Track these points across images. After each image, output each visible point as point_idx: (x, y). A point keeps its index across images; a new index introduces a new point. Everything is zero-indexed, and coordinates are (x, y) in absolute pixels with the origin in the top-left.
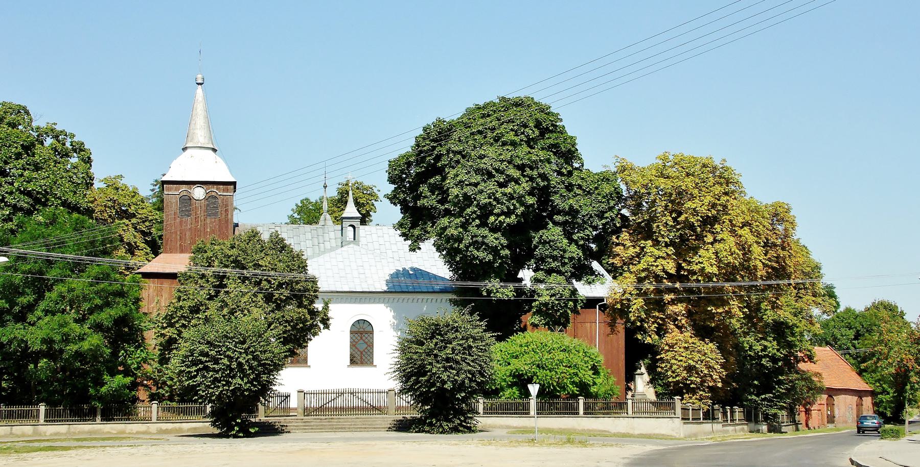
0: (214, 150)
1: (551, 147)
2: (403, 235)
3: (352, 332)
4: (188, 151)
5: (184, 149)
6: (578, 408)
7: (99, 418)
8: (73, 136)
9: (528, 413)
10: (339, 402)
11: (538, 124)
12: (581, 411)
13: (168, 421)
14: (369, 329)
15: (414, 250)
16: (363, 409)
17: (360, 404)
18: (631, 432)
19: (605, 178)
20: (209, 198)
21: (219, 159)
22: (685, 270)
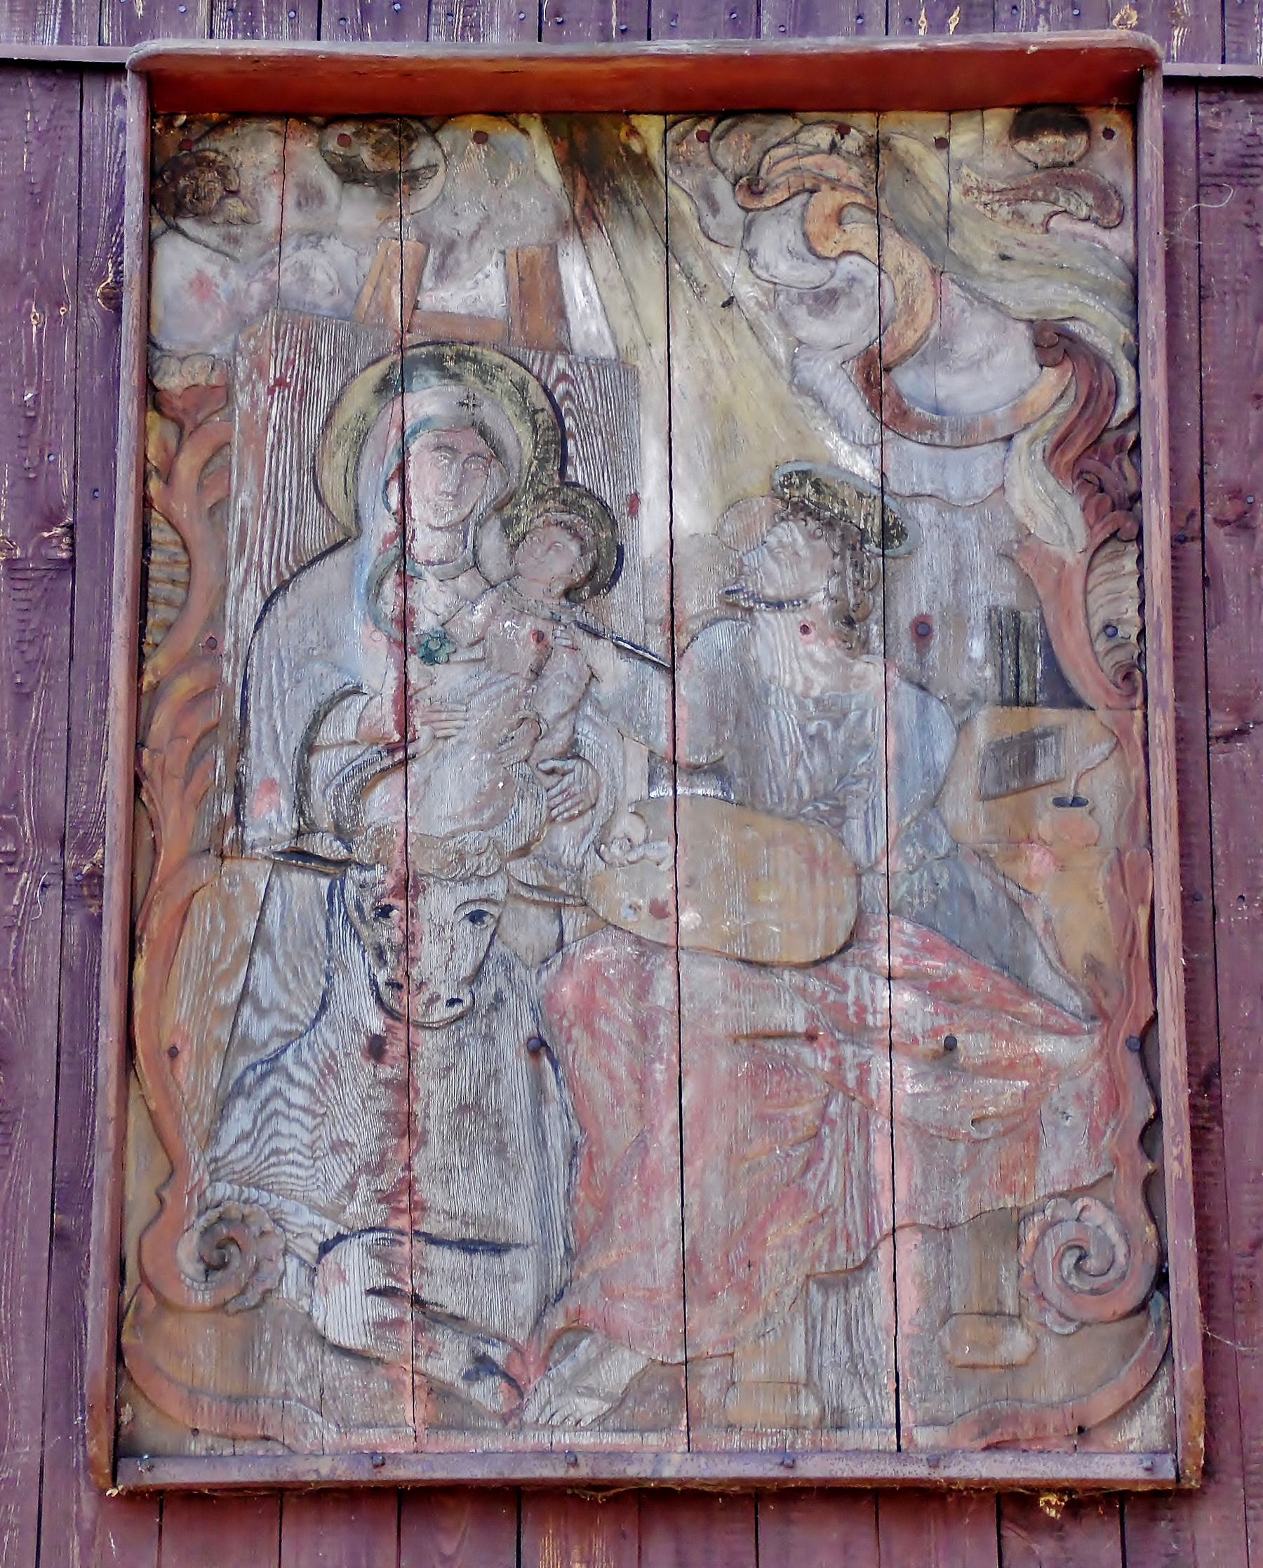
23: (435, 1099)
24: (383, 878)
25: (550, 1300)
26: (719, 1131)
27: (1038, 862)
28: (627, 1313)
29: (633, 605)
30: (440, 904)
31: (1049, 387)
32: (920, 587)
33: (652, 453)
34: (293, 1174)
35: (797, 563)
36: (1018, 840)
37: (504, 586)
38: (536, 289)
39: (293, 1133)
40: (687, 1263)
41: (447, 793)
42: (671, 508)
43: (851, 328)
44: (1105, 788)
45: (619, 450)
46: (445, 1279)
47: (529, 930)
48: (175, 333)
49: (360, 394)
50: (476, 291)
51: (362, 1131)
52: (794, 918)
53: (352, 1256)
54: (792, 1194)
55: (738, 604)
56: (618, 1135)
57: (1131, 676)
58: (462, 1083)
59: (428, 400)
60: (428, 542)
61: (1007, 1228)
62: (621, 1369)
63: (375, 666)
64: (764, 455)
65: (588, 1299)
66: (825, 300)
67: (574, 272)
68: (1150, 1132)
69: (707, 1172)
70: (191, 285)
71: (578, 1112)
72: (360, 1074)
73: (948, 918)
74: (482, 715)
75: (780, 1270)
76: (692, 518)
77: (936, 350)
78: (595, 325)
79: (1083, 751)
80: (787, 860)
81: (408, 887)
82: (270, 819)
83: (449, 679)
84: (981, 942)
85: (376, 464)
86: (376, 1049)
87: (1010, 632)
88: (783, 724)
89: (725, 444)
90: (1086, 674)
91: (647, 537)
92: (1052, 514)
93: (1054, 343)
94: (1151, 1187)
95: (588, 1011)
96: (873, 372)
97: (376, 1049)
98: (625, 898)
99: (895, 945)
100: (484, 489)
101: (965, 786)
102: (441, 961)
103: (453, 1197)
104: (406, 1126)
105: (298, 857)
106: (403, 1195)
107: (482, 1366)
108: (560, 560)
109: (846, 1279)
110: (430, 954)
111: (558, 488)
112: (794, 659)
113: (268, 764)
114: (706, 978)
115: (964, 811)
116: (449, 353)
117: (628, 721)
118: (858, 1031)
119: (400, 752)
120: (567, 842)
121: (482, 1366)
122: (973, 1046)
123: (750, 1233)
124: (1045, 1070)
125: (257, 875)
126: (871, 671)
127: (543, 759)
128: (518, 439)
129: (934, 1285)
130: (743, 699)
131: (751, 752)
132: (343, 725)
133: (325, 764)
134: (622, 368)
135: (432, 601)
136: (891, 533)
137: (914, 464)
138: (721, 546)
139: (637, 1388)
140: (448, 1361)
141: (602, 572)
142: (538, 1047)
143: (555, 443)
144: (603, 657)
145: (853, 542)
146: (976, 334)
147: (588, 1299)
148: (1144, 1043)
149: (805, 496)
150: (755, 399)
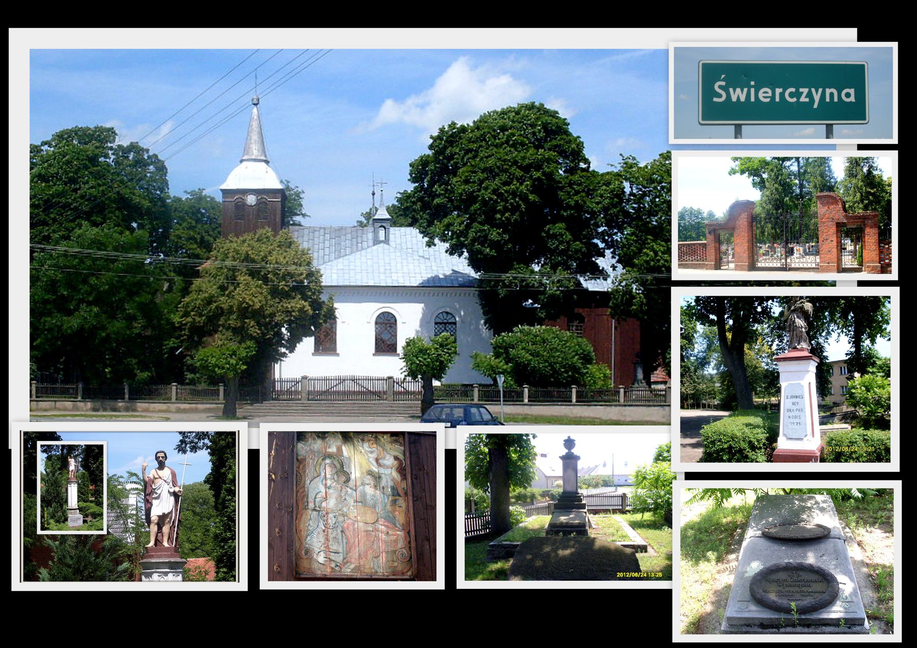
0: (267, 162)
1: (554, 148)
2: (421, 232)
3: (376, 323)
4: (244, 163)
5: (242, 161)
6: (571, 397)
7: (823, 414)
8: (147, 151)
9: (571, 401)
10: (341, 388)
11: (545, 126)
12: (574, 400)
13: (185, 401)
14: (393, 321)
15: (430, 246)
16: (359, 393)
17: (357, 389)
18: (622, 419)
19: (608, 179)
20: (259, 203)
21: (269, 169)
22: (569, 207)
23: (331, 536)
24: (324, 513)
25: (344, 559)
26: (363, 541)
27: (397, 513)
28: (353, 560)
29: (351, 484)
30: (331, 515)
31: (396, 462)
32: (383, 483)
33: (208, 406)
34: (315, 544)
35: (369, 480)
36: (394, 511)
37: (337, 481)
38: (339, 449)
39: (315, 540)
40: (360, 555)
41: (331, 503)
42: (356, 473)
43: (374, 455)
44: (404, 505)
45: (349, 467)
46: (333, 556)
47: (341, 519)
48: (300, 453)
49: (320, 460)
50: (333, 449)
51: (322, 540)
52: (370, 518)
53: (322, 553)
54: (371, 548)
55: (363, 484)
56: (352, 541)
57: (406, 494)
58: (334, 535)
59: (328, 461)
60: (328, 476)
61: (395, 552)
62: (352, 566)
63: (323, 489)
64: (366, 468)
65: (348, 559)
66: (371, 452)
67: (343, 448)
68: (410, 542)
69: (361, 545)
70: (715, 592)
71: (347, 539)
72: (322, 534)
73: (387, 519)
74: (334, 496)
75: (370, 556)
76: (358, 475)
77: (384, 458)
78: (526, 390)
79: (401, 501)
80: (369, 512)
81: (327, 513)
82: (311, 505)
83: (331, 491)
84: (391, 520)
85: (322, 467)
86: (324, 531)
87: (393, 488)
88: (368, 497)
89: (361, 467)
90: (401, 493)
91: (353, 477)
92: (396, 475)
93: (396, 458)
94: (410, 548)
95: (348, 528)
96: (377, 460)
97: (324, 531)
98: (352, 516)
99: (381, 521)
100: (334, 471)
101: (389, 504)
102: (331, 521)
103: (334, 547)
104: (327, 539)
105: (314, 510)
106: (327, 547)
107: (337, 566)
108: (344, 479)
109: (377, 557)
110: (330, 521)
111: (342, 471)
112: (370, 490)
113: (311, 499)
114: (361, 524)
115: (389, 507)
116: (330, 456)
117: (351, 496)
118: (378, 531)
119: (326, 499)
120: (345, 509)
121: (337, 566)
122: (390, 532)
123: (366, 552)
124: (398, 535)
125: (310, 512)
126: (378, 492)
127: (341, 500)
128: (338, 466)
129: (387, 558)
130: (364, 495)
131: (365, 500)
132: (319, 496)
133: (317, 500)
134: (350, 458)
135: (329, 482)
136: (380, 477)
137: (382, 470)
138: (361, 478)
139: (354, 568)
140: (333, 565)
141: (348, 480)
142: (342, 531)
143: (342, 466)
144: (348, 489)
145: (376, 478)
146: (388, 457)
147: (348, 559)
148: (409, 533)
149: (370, 473)
150: (364, 462)
